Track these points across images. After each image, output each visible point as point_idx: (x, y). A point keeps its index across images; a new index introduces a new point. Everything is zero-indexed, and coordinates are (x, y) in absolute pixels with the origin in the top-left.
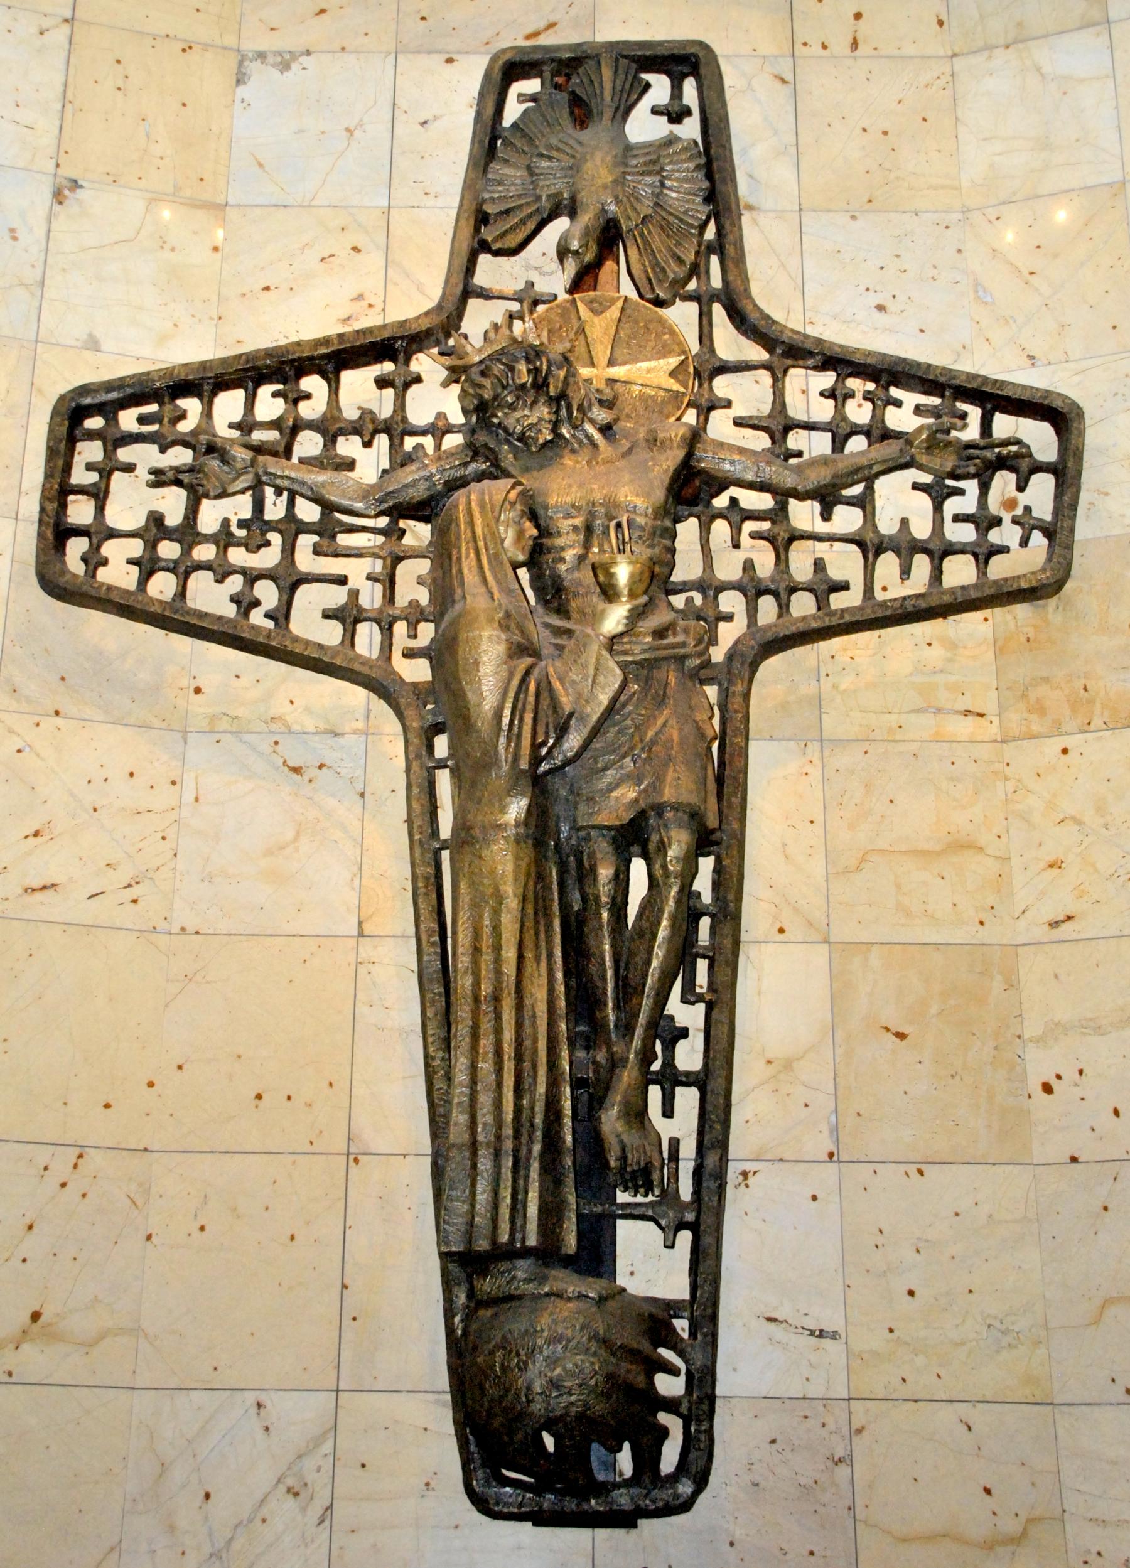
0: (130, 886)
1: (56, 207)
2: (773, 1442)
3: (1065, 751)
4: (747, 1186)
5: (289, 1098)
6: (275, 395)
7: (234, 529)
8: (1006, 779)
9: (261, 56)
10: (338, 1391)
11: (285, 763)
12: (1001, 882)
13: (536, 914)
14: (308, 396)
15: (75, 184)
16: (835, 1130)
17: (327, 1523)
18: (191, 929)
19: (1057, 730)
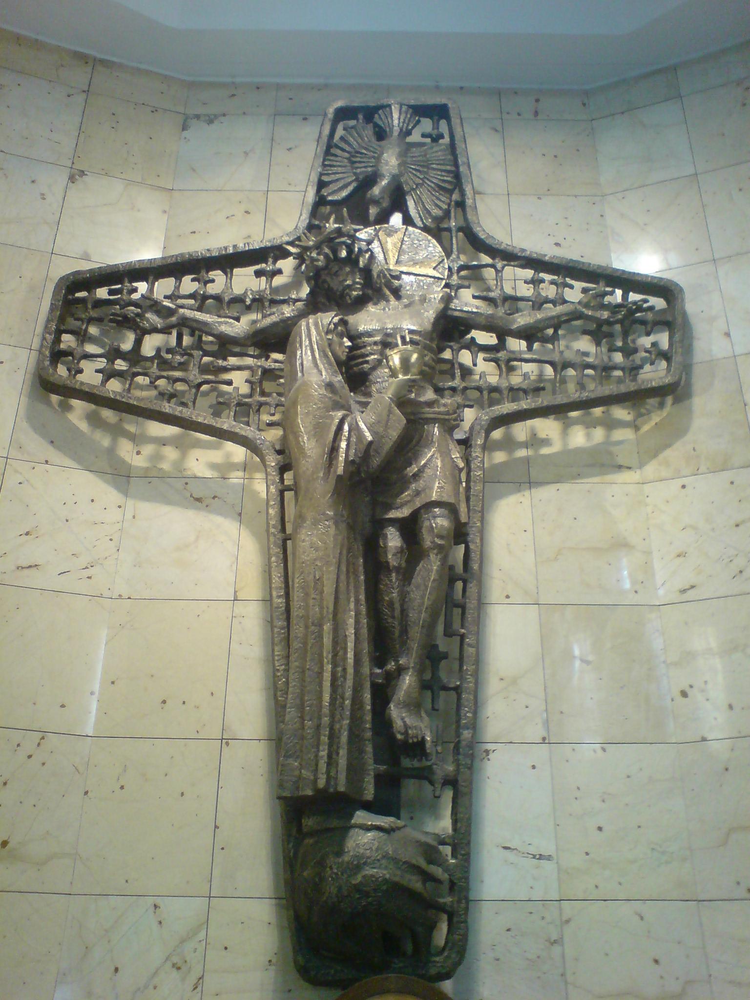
0: (87, 568)
1: (70, 184)
2: (508, 930)
4: (489, 760)
5: (184, 703)
8: (647, 505)
9: (198, 117)
10: (210, 897)
11: (191, 496)
12: (647, 567)
13: (348, 571)
14: (213, 281)
15: (82, 173)
16: (547, 723)
17: (199, 989)
18: (125, 596)
19: (678, 475)
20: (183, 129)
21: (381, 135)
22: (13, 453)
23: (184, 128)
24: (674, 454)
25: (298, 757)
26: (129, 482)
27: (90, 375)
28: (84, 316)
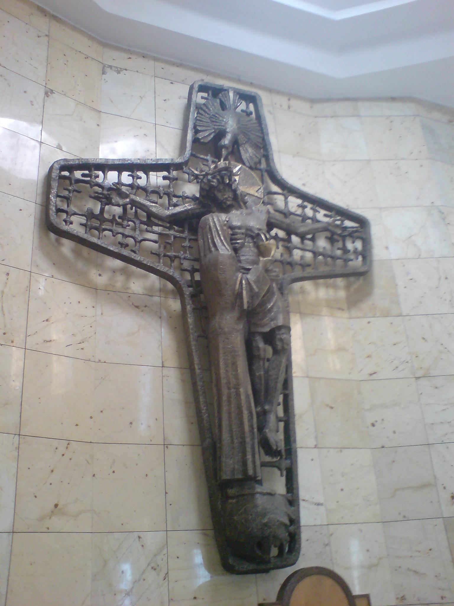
1: (46, 98)
3: (369, 322)
6: (129, 175)
7: (117, 218)
9: (110, 67)
15: (52, 92)
16: (316, 438)
19: (365, 316)
20: (103, 73)
21: (223, 106)
22: (34, 270)
23: (104, 73)
24: (365, 306)
25: (231, 458)
26: (97, 293)
27: (76, 226)
28: (70, 188)
